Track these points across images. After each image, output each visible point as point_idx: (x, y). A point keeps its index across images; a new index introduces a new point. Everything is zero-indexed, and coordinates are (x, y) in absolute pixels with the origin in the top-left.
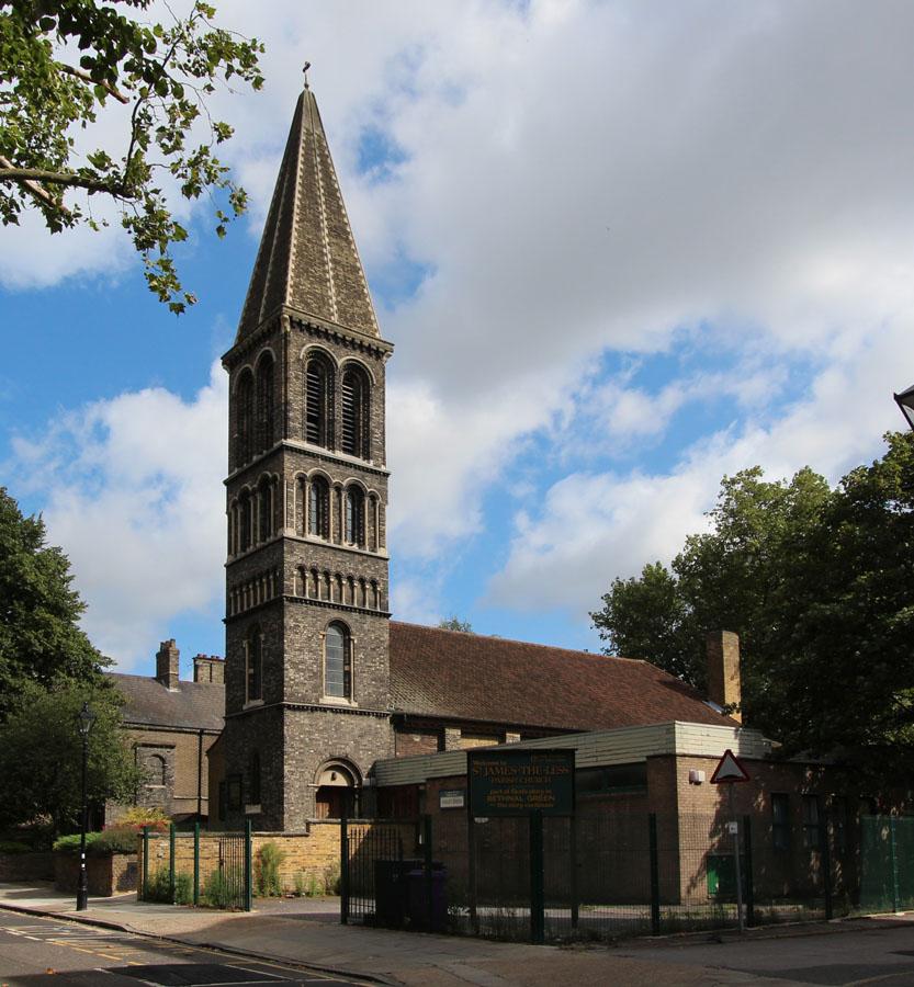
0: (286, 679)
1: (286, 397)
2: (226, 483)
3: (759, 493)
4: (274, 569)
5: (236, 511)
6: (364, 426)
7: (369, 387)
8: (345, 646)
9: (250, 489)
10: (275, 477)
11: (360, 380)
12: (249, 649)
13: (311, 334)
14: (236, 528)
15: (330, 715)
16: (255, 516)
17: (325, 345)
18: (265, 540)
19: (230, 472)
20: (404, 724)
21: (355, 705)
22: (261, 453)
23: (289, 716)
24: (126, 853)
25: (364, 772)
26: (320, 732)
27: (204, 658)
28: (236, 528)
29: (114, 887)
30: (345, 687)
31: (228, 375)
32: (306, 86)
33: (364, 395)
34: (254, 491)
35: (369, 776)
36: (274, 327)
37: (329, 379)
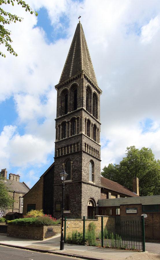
0: (82, 174)
1: (83, 96)
2: (56, 120)
3: (135, 151)
4: (77, 143)
5: (60, 128)
6: (96, 110)
7: (97, 100)
8: (92, 167)
9: (67, 121)
10: (78, 118)
11: (95, 98)
12: (65, 165)
13: (88, 81)
14: (60, 132)
15: (90, 185)
16: (68, 129)
17: (90, 86)
18: (72, 136)
19: (57, 117)
20: (104, 191)
21: (95, 184)
22: (71, 112)
23: (30, 188)
24: (47, 225)
25: (96, 202)
26: (89, 190)
27: (12, 174)
28: (60, 132)
29: (44, 237)
30: (92, 179)
31: (56, 92)
32: (80, 22)
33: (96, 102)
34: (68, 122)
35: (97, 203)
36: (78, 76)
37: (90, 95)
